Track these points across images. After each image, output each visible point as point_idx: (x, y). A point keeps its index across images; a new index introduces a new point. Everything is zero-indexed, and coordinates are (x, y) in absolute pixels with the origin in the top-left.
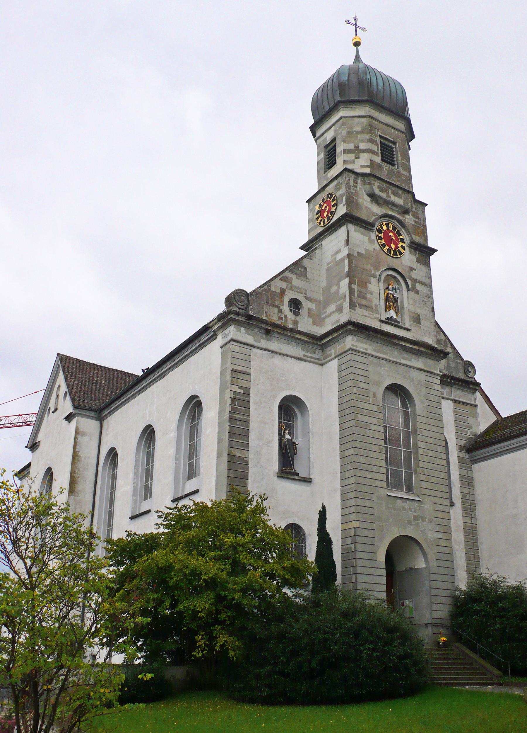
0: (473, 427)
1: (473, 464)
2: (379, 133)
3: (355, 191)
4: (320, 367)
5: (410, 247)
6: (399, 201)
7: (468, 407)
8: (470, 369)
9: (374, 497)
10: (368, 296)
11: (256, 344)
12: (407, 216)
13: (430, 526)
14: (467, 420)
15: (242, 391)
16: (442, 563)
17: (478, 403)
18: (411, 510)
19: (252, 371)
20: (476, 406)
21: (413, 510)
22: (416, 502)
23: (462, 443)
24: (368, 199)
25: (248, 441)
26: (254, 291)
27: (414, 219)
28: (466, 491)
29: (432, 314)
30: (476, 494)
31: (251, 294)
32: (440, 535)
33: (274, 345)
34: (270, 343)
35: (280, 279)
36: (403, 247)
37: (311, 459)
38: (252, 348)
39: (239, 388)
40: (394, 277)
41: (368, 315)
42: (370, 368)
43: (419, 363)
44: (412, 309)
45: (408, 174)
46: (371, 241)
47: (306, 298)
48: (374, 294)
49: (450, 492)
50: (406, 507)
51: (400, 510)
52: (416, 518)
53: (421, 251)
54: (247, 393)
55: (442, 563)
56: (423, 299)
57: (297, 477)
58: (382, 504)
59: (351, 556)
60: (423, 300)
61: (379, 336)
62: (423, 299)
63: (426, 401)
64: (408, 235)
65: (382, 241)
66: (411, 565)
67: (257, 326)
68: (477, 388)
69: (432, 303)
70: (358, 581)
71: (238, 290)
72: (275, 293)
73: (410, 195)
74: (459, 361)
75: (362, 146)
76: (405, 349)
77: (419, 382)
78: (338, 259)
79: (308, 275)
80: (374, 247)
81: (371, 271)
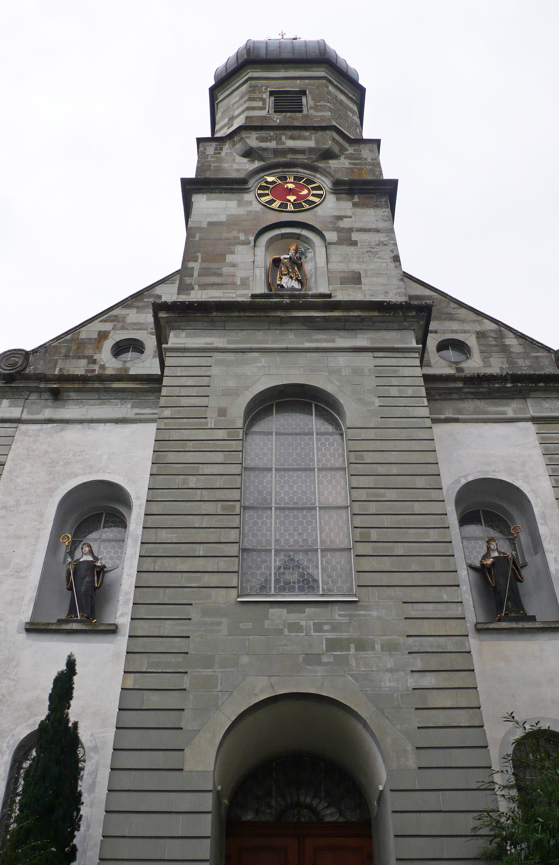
9: (194, 613)
11: (25, 416)
22: (336, 607)
24: (245, 160)
32: (428, 680)
33: (70, 411)
42: (215, 371)
50: (303, 623)
51: (280, 632)
53: (362, 192)
58: (220, 624)
64: (326, 177)
67: (31, 390)
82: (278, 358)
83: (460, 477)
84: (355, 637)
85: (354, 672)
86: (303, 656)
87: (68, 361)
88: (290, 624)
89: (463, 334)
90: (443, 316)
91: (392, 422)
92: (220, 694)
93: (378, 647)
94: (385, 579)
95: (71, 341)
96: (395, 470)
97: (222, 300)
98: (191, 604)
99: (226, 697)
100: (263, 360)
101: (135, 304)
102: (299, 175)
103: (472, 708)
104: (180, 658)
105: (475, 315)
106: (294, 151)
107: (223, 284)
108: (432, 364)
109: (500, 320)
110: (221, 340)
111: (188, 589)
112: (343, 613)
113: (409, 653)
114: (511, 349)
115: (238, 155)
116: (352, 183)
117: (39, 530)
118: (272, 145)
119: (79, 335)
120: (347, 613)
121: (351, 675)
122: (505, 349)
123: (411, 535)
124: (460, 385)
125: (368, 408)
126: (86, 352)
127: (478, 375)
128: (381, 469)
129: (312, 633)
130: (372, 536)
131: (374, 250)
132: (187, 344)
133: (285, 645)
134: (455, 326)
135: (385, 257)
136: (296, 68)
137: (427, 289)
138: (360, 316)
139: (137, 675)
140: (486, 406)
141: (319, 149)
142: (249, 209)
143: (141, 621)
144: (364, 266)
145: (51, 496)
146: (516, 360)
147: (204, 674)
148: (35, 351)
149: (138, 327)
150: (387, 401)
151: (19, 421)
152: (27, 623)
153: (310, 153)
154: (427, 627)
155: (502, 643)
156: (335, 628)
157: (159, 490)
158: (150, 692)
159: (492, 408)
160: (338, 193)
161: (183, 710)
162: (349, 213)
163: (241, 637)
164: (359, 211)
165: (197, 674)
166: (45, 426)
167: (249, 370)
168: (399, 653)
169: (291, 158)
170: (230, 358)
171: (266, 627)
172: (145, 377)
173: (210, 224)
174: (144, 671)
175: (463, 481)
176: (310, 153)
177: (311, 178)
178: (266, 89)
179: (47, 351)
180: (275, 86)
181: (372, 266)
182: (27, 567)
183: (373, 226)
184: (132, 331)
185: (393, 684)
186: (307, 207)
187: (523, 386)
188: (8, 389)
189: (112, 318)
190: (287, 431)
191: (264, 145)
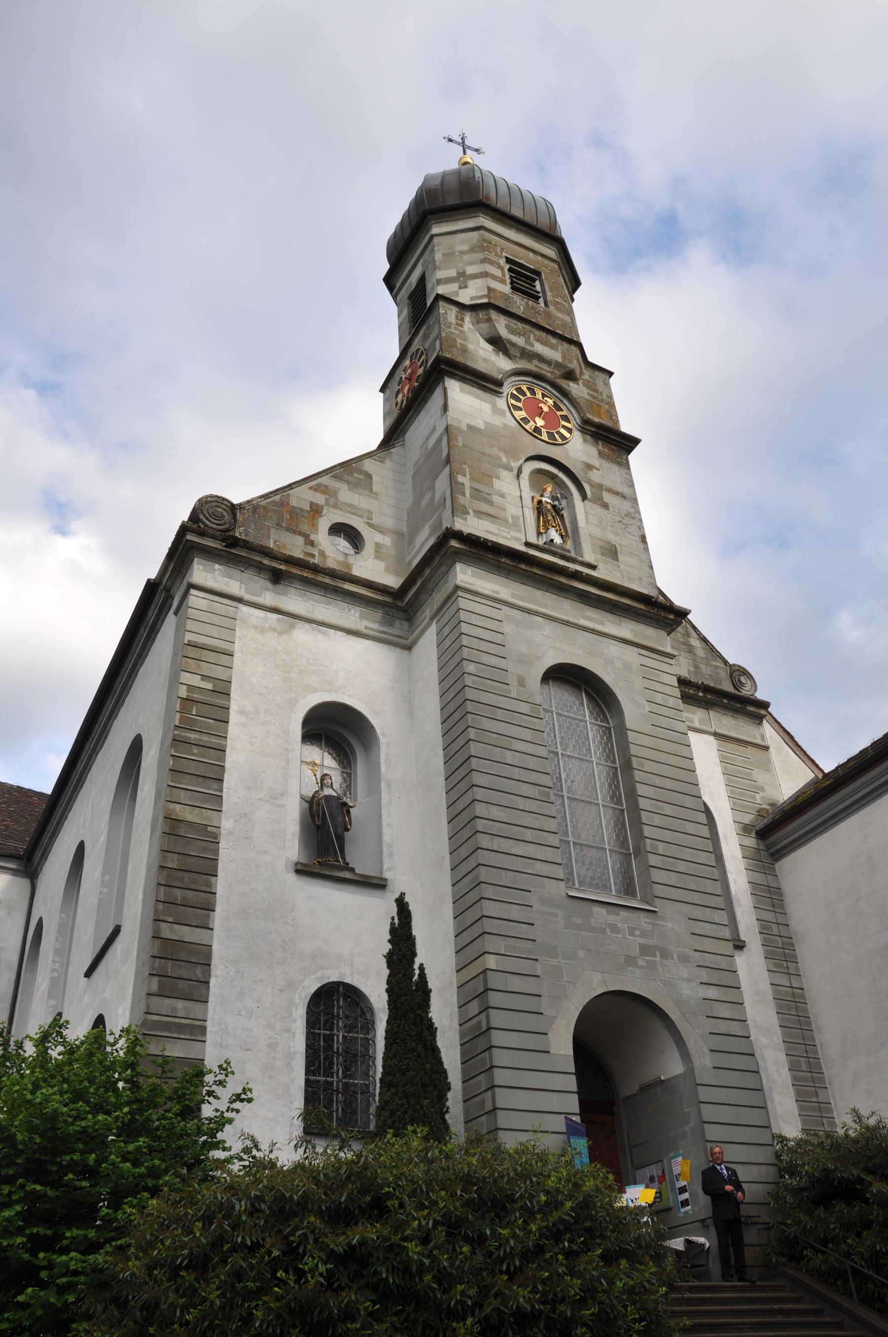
0: (766, 787)
1: (777, 860)
2: (504, 254)
3: (461, 332)
4: (405, 652)
5: (583, 430)
6: (555, 355)
7: (750, 749)
8: (743, 679)
10: (496, 499)
11: (247, 597)
12: (572, 384)
13: (685, 972)
14: (750, 775)
15: (209, 686)
16: (724, 1060)
17: (769, 742)
18: (632, 933)
19: (237, 648)
20: (766, 748)
21: (637, 932)
22: (642, 914)
23: (748, 819)
24: (489, 348)
25: (221, 791)
26: (248, 502)
27: (587, 391)
28: (769, 916)
29: (641, 546)
30: (792, 923)
31: (241, 506)
32: (713, 993)
33: (295, 600)
34: (283, 598)
35: (310, 488)
36: (570, 431)
37: (386, 837)
38: (240, 606)
39: (202, 680)
40: (553, 477)
41: (496, 532)
42: (507, 628)
43: (626, 629)
44: (598, 532)
45: (568, 319)
46: (495, 410)
47: (370, 525)
48: (507, 497)
49: (719, 858)
50: (619, 925)
51: (603, 931)
52: (646, 950)
54: (223, 690)
55: (724, 1060)
56: (620, 519)
57: (347, 875)
59: (481, 1044)
60: (620, 522)
61: (523, 566)
62: (620, 519)
63: (647, 704)
65: (522, 414)
66: (648, 1077)
68: (763, 712)
69: (641, 528)
70: (498, 1106)
71: (211, 496)
72: (298, 511)
73: (573, 347)
74: (717, 664)
75: (471, 270)
76: (585, 598)
77: (627, 666)
78: (429, 447)
79: (375, 488)
80: (505, 422)
81: (499, 458)
82: (560, 628)
91: (660, 732)
101: (345, 476)
104: (530, 945)
110: (505, 590)
114: (696, 651)
117: (287, 750)
121: (660, 980)
136: (519, 230)
141: (565, 367)
143: (492, 902)
145: (293, 710)
149: (353, 511)
151: (240, 600)
153: (554, 368)
156: (643, 934)
166: (269, 615)
172: (381, 587)
184: (347, 515)
185: (689, 993)
189: (323, 488)
191: (514, 339)
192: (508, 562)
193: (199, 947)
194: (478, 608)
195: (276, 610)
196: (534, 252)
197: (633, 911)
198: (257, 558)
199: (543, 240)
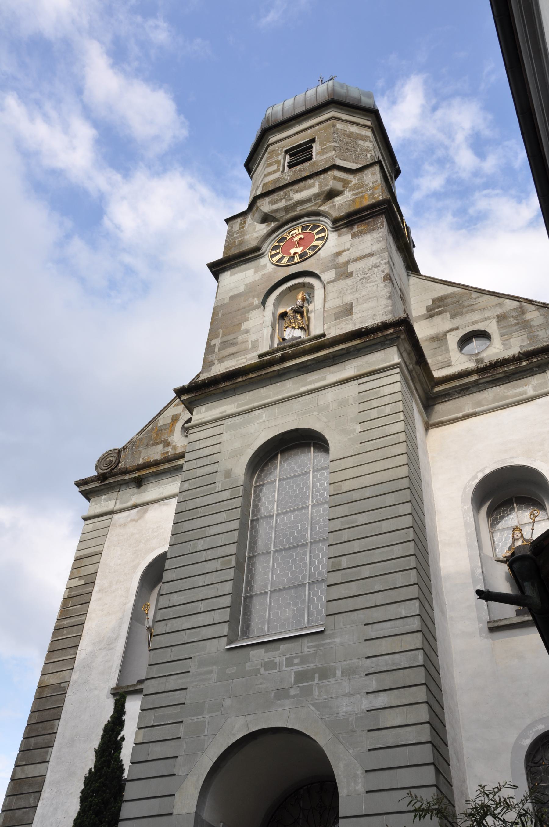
9: (192, 666)
11: (118, 506)
15: (82, 582)
22: (305, 640)
32: (382, 700)
40: (290, 289)
50: (277, 660)
58: (211, 672)
82: (276, 409)
83: (478, 472)
84: (319, 666)
85: (316, 701)
86: (275, 691)
87: (149, 449)
88: (267, 663)
89: (483, 323)
90: (465, 310)
92: (206, 738)
93: (339, 673)
94: (350, 604)
95: (153, 429)
96: (368, 493)
97: (236, 367)
98: (191, 658)
99: (210, 740)
100: (264, 415)
102: (307, 224)
103: (421, 724)
105: (496, 298)
106: (301, 202)
107: (237, 353)
108: (453, 363)
109: (520, 296)
110: (233, 406)
111: (190, 645)
112: (311, 644)
113: (367, 675)
115: (258, 223)
116: (349, 215)
118: (282, 204)
119: (157, 424)
120: (314, 644)
121: (313, 705)
122: (525, 325)
123: (377, 555)
124: (475, 377)
125: (350, 437)
126: (163, 437)
127: (490, 363)
128: (356, 496)
129: (284, 669)
130: (343, 563)
131: (366, 276)
132: (206, 417)
133: (261, 684)
134: (476, 316)
135: (377, 279)
136: (300, 123)
137: (450, 287)
138: (344, 349)
139: (146, 729)
140: (506, 391)
142: (264, 272)
143: (153, 680)
144: (357, 295)
146: (538, 333)
147: (195, 720)
148: (124, 448)
150: (367, 425)
151: (112, 512)
152: (112, 689)
153: (315, 199)
154: (385, 646)
155: (516, 638)
157: (175, 559)
158: (154, 744)
159: (511, 392)
160: (339, 230)
161: (177, 757)
162: (348, 246)
163: (226, 682)
164: (357, 240)
165: (190, 721)
167: (252, 428)
168: (357, 676)
169: (300, 210)
170: (238, 421)
171: (247, 668)
173: (232, 298)
174: (151, 725)
175: (481, 476)
176: (315, 199)
177: (317, 223)
178: (282, 150)
179: (134, 445)
180: (289, 144)
181: (364, 293)
182: (116, 639)
183: (367, 251)
185: (350, 709)
186: (312, 253)
187: (538, 361)
188: (103, 487)
190: (289, 476)
191: (275, 207)
192: (227, 384)
193: (36, 778)
194: (202, 435)
195: (135, 506)
196: (318, 124)
197: (296, 640)
198: (120, 478)
199: (321, 112)
